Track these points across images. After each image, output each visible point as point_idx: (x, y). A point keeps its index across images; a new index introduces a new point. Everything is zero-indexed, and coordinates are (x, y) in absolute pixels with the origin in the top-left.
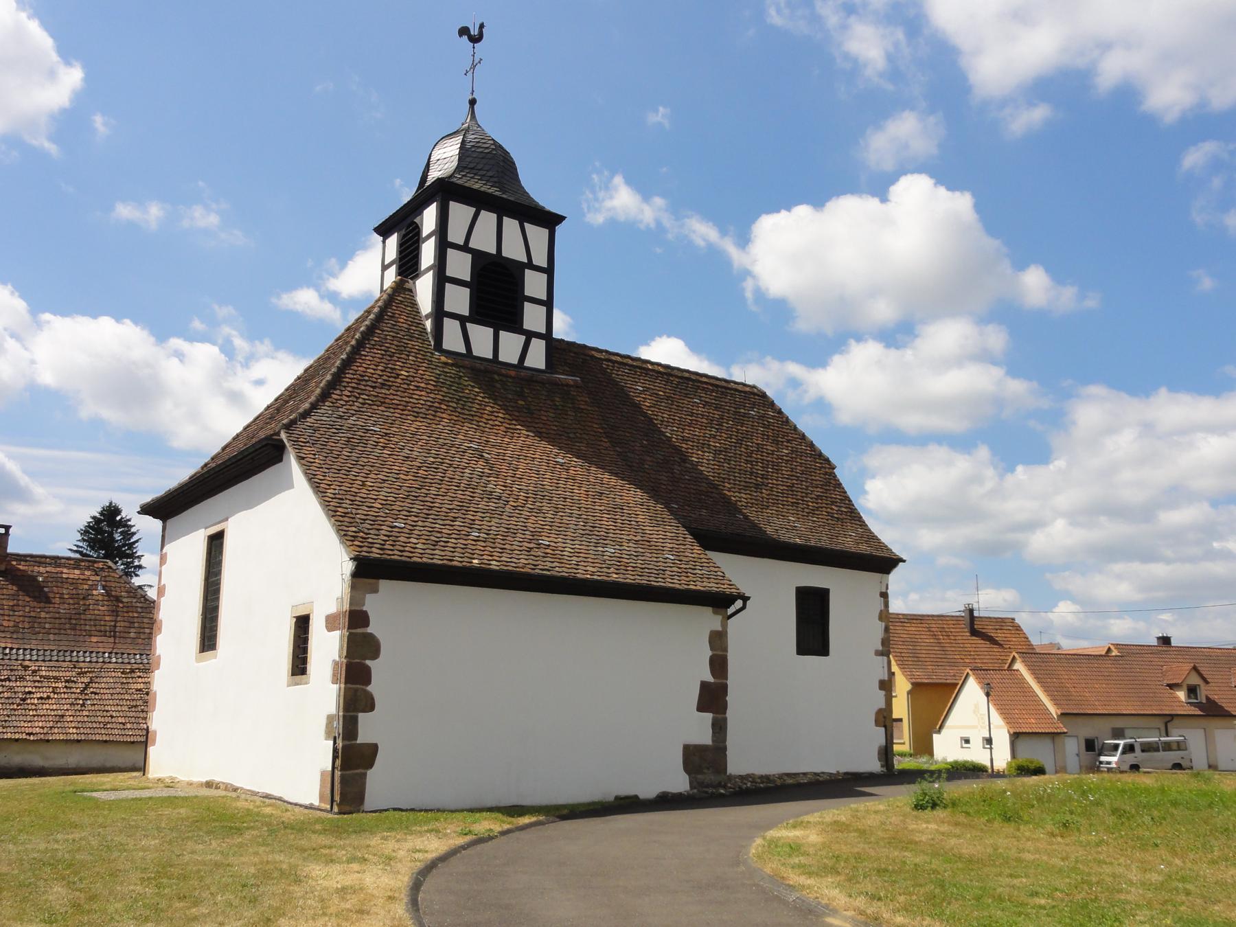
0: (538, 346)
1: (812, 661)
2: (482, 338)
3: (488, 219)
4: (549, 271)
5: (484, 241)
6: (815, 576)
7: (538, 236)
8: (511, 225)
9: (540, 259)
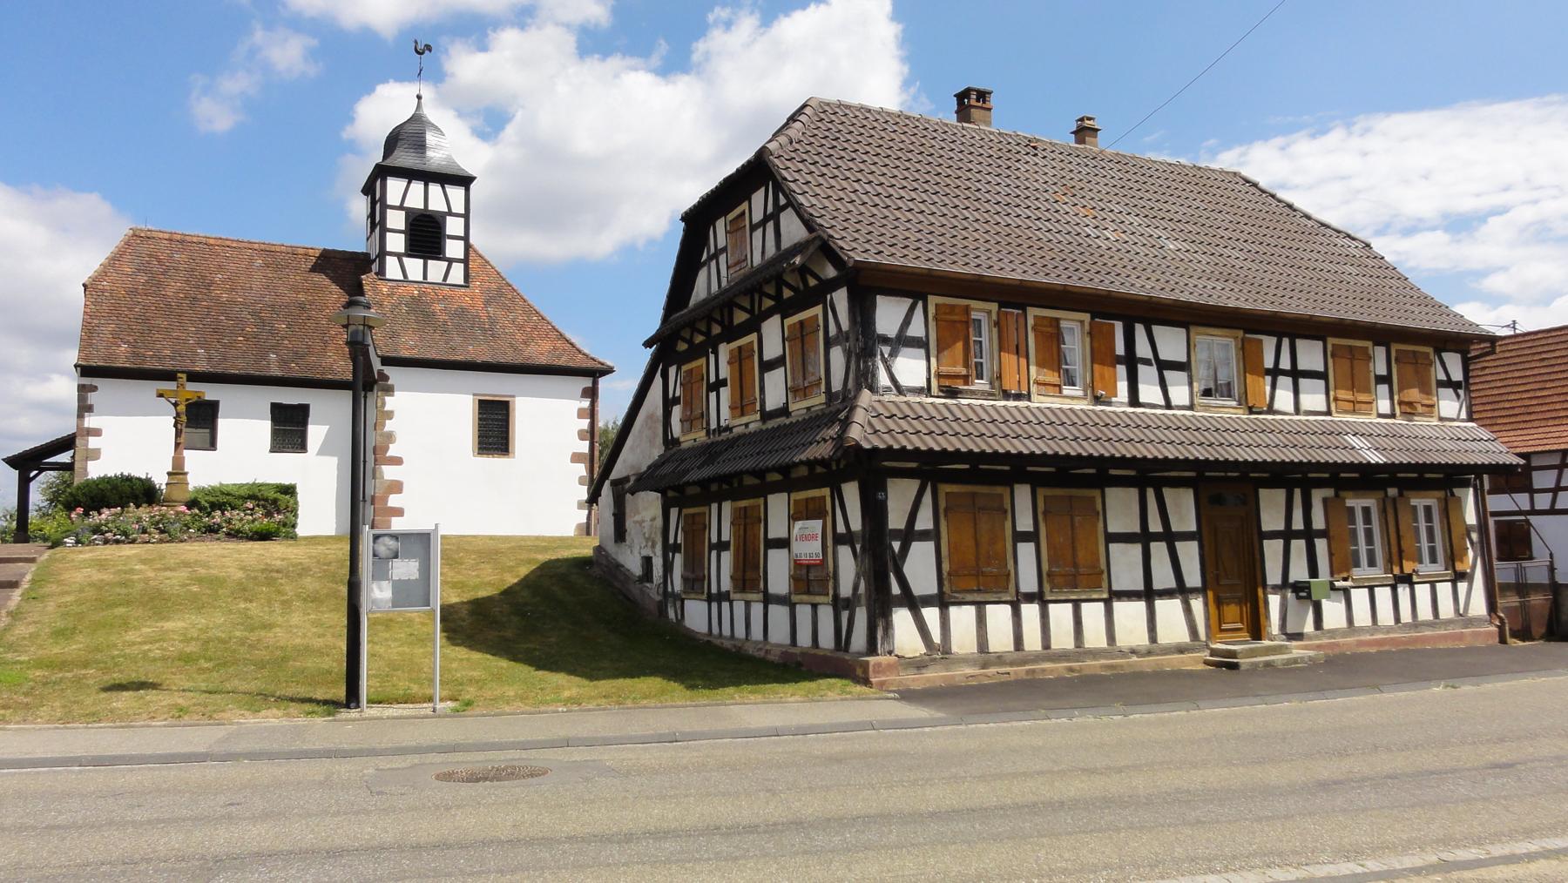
1: (494, 462)
2: (414, 266)
3: (417, 187)
4: (466, 216)
5: (415, 200)
6: (495, 386)
7: (456, 193)
8: (435, 189)
9: (458, 207)
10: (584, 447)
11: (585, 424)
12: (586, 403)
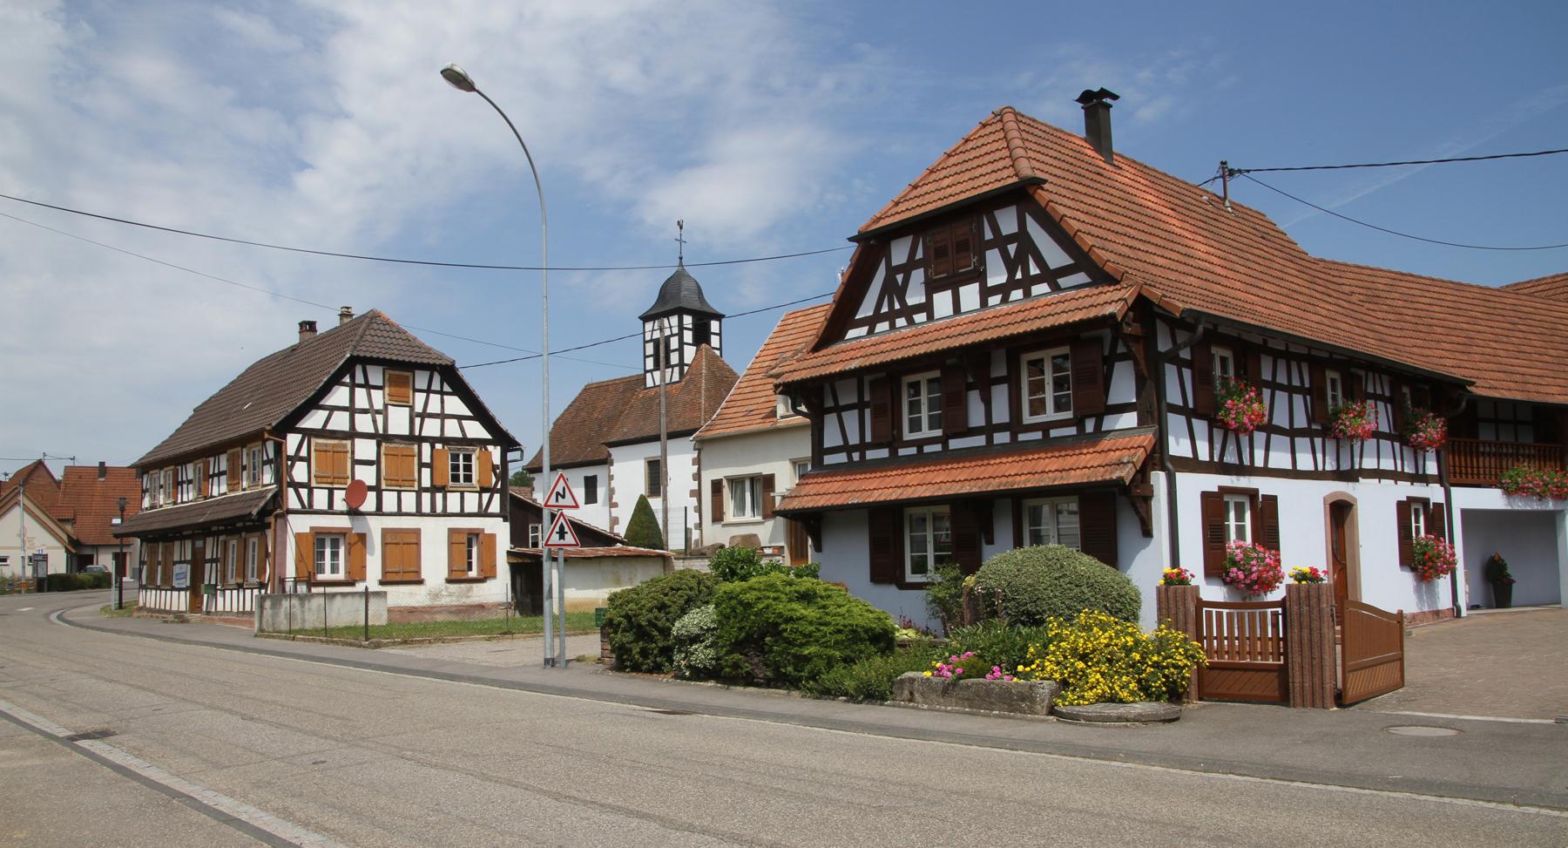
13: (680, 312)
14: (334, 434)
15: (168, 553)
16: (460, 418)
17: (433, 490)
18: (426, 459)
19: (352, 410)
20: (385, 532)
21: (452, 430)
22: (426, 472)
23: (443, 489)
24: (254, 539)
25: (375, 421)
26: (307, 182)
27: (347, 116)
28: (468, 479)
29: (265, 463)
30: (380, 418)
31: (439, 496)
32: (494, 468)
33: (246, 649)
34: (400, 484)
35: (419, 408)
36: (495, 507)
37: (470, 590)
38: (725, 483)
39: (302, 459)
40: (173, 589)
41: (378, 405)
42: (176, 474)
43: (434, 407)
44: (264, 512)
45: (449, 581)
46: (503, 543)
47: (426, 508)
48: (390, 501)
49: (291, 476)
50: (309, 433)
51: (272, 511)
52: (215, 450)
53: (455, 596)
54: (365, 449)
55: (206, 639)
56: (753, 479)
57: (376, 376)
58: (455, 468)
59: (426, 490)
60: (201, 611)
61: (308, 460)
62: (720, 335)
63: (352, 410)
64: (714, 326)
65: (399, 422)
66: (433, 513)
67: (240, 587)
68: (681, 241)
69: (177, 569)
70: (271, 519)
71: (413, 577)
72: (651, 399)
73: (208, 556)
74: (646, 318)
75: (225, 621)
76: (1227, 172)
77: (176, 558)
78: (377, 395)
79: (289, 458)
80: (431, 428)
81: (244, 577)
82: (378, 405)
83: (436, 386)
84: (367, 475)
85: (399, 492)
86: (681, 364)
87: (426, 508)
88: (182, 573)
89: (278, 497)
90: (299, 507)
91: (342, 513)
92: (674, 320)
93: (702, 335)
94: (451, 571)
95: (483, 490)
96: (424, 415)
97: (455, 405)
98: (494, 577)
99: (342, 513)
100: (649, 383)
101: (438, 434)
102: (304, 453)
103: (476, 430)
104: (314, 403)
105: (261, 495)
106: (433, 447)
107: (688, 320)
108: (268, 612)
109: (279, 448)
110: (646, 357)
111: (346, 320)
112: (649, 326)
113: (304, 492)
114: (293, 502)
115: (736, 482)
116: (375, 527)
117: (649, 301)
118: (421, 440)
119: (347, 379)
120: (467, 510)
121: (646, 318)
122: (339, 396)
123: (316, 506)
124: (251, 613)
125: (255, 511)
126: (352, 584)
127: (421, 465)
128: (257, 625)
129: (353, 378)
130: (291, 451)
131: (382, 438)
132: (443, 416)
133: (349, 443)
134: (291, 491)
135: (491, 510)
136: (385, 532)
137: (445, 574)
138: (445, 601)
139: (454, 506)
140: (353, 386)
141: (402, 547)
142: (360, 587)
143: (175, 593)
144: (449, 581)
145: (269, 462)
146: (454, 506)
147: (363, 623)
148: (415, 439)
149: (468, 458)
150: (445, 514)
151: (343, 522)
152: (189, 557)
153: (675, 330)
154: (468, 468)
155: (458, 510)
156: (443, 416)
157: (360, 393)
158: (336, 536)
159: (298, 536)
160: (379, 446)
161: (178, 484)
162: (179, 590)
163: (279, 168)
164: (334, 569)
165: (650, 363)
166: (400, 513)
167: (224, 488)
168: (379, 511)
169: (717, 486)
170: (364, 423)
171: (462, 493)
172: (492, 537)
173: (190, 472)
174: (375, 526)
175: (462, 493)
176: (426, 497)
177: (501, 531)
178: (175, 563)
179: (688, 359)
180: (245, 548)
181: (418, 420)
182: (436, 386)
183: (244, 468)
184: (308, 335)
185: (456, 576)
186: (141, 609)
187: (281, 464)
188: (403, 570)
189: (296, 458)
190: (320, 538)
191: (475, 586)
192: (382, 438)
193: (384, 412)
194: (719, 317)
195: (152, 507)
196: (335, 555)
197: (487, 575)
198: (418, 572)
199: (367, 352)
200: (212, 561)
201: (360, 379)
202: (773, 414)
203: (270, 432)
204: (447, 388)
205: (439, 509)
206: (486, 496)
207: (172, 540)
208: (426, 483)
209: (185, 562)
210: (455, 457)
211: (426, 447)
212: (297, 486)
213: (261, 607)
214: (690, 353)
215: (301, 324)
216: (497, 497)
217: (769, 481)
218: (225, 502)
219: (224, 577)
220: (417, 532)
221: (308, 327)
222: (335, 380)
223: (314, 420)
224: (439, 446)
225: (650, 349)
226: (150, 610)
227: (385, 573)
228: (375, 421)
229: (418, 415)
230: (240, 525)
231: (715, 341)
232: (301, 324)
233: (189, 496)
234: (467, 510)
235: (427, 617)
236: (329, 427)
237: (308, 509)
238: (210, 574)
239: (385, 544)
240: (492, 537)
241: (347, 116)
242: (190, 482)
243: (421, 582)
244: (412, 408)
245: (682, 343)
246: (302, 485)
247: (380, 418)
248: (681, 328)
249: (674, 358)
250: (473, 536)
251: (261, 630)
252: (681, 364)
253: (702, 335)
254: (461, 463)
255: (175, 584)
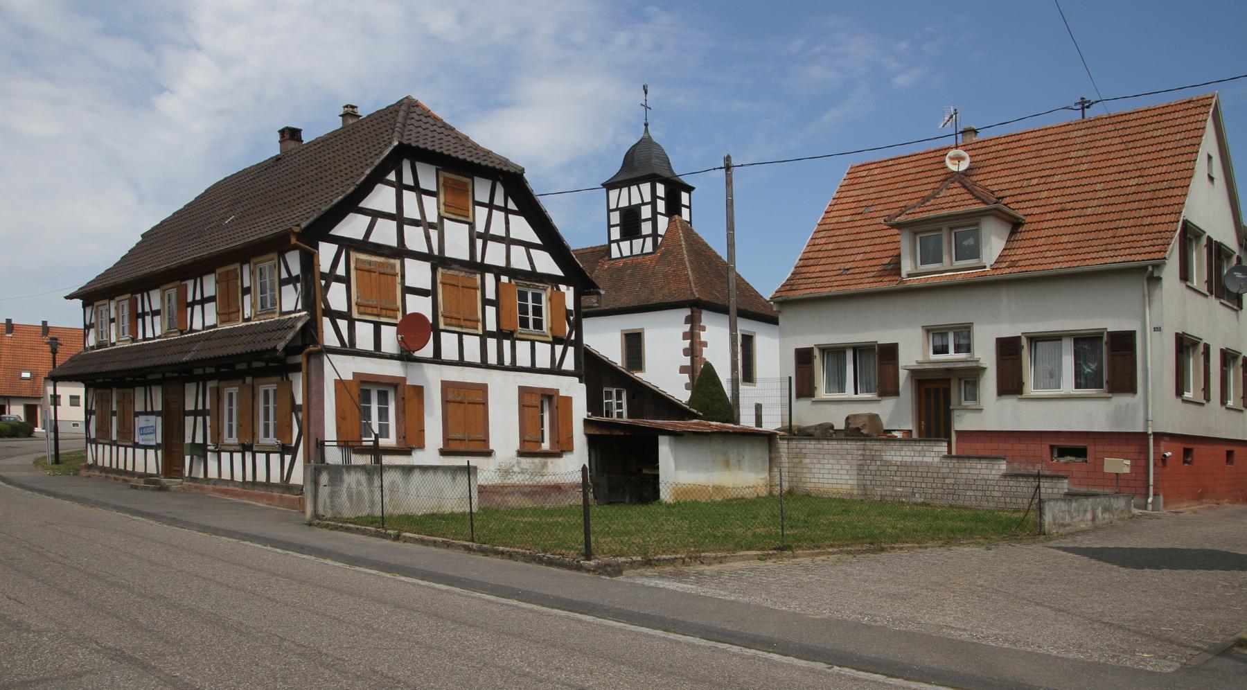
0: (649, 241)
10: (687, 361)
11: (687, 343)
12: (687, 328)
13: (653, 179)
14: (378, 249)
15: (127, 402)
16: (528, 246)
17: (500, 335)
18: (491, 294)
19: (399, 219)
20: (446, 386)
21: (519, 260)
22: (491, 311)
23: (511, 335)
24: (269, 387)
25: (428, 238)
26: (167, 104)
27: (199, 48)
28: (538, 324)
29: (283, 282)
30: (434, 234)
31: (507, 344)
32: (568, 313)
33: (287, 546)
34: (464, 323)
35: (480, 228)
36: (569, 364)
37: (544, 466)
38: (816, 352)
39: (339, 279)
40: (136, 446)
41: (432, 217)
42: (133, 305)
43: (497, 228)
44: (291, 350)
45: (521, 454)
46: (580, 411)
47: (492, 359)
48: (449, 343)
49: (326, 301)
50: (346, 245)
51: (299, 349)
52: (197, 270)
53: (526, 472)
54: (418, 274)
55: (254, 528)
56: (860, 350)
57: (428, 179)
58: (524, 310)
59: (492, 335)
60: (181, 475)
61: (346, 280)
62: (689, 207)
63: (399, 219)
64: (685, 198)
65: (457, 242)
66: (500, 366)
67: (244, 448)
68: (646, 107)
69: (141, 422)
70: (300, 359)
71: (480, 448)
72: (619, 269)
73: (189, 406)
74: (609, 186)
75: (225, 492)
76: (1084, 105)
77: (139, 407)
78: (430, 203)
79: (323, 276)
80: (495, 255)
81: (254, 435)
82: (432, 217)
83: (499, 201)
84: (420, 306)
85: (460, 335)
86: (655, 234)
87: (492, 359)
88: (150, 428)
89: (310, 332)
90: (337, 344)
91: (392, 357)
92: (646, 188)
93: (674, 208)
94: (523, 441)
95: (556, 340)
96: (487, 237)
97: (521, 228)
98: (570, 450)
99: (392, 357)
100: (615, 253)
101: (502, 263)
102: (341, 271)
103: (546, 263)
104: (351, 204)
105: (283, 326)
106: (498, 280)
107: (661, 190)
108: (324, 492)
109: (309, 261)
110: (610, 226)
111: (351, 121)
112: (614, 194)
113: (343, 324)
114: (329, 338)
115: (834, 353)
116: (432, 378)
117: (613, 168)
118: (484, 268)
119: (392, 177)
120: (538, 365)
121: (609, 186)
122: (382, 198)
123: (360, 345)
124: (299, 490)
125: (281, 346)
126: (407, 452)
127: (486, 302)
128: (309, 509)
129: (399, 175)
130: (325, 264)
131: (438, 261)
132: (508, 241)
133: (397, 262)
134: (326, 322)
135: (564, 367)
136: (446, 386)
137: (516, 444)
138: (517, 479)
139: (543, 361)
140: (400, 187)
141: (466, 405)
142: (418, 458)
143: (140, 452)
144: (521, 454)
145: (292, 280)
146: (523, 359)
147: (468, 510)
148: (476, 267)
149: (537, 298)
150: (514, 368)
151: (393, 369)
152: (158, 407)
153: (648, 198)
154: (537, 311)
155: (528, 364)
156: (508, 241)
157: (409, 198)
158: (386, 386)
159: (340, 383)
160: (434, 270)
161: (136, 316)
162: (146, 447)
163: (140, 92)
164: (384, 432)
165: (616, 233)
166: (461, 363)
167: (211, 319)
168: (437, 359)
169: (804, 358)
170: (415, 239)
171: (533, 343)
172: (568, 400)
173: (155, 299)
174: (432, 378)
175: (533, 343)
176: (492, 343)
177: (575, 391)
178: (137, 414)
179: (662, 230)
180: (254, 397)
181: (479, 242)
182: (499, 201)
183: (246, 291)
184: (292, 145)
185: (527, 449)
186: (90, 467)
187: (312, 284)
188: (468, 437)
189: (331, 277)
190: (363, 388)
191: (550, 461)
192: (438, 261)
193: (439, 226)
194: (689, 189)
195: (100, 345)
196: (383, 414)
197: (562, 447)
198: (486, 441)
199: (403, 144)
200: (195, 413)
201: (408, 179)
202: (895, 268)
203: (300, 236)
204: (512, 205)
205: (507, 361)
206: (559, 349)
207: (133, 385)
208: (492, 326)
209: (152, 413)
210: (523, 296)
211: (490, 278)
212: (334, 315)
213: (316, 483)
214: (663, 223)
215: (282, 132)
216: (571, 350)
217: (889, 353)
218: (211, 336)
219: (217, 434)
220: (483, 388)
221: (290, 134)
222: (377, 177)
223: (353, 227)
224: (504, 279)
225: (616, 218)
226: (103, 469)
227: (446, 440)
228: (428, 238)
229: (480, 236)
230: (242, 366)
231: (685, 212)
232: (282, 132)
233: (154, 329)
234: (538, 365)
235: (498, 499)
236: (372, 239)
237: (348, 349)
238: (193, 432)
239: (445, 401)
240: (568, 400)
241: (199, 48)
242: (155, 313)
243: (488, 454)
244: (472, 225)
245: (655, 212)
246: (341, 315)
247: (434, 234)
248: (654, 196)
249: (646, 228)
250: (549, 396)
251: (316, 515)
252: (655, 234)
253: (674, 208)
254: (530, 304)
255: (139, 439)
